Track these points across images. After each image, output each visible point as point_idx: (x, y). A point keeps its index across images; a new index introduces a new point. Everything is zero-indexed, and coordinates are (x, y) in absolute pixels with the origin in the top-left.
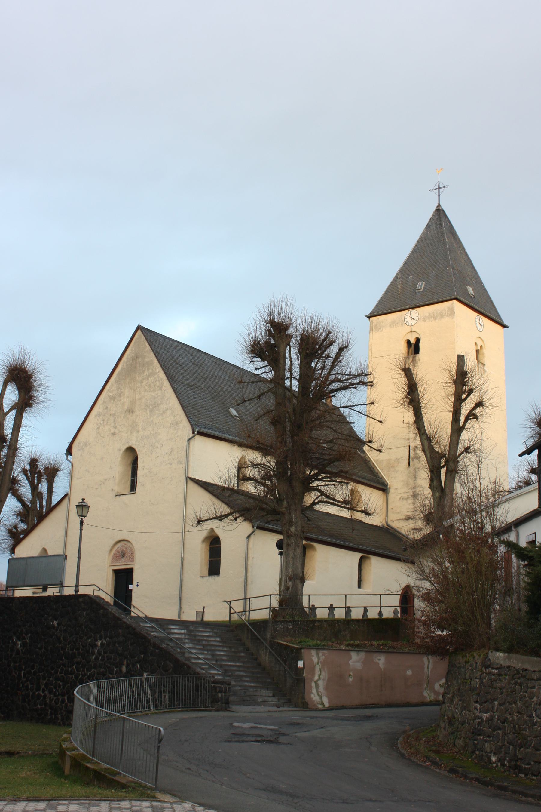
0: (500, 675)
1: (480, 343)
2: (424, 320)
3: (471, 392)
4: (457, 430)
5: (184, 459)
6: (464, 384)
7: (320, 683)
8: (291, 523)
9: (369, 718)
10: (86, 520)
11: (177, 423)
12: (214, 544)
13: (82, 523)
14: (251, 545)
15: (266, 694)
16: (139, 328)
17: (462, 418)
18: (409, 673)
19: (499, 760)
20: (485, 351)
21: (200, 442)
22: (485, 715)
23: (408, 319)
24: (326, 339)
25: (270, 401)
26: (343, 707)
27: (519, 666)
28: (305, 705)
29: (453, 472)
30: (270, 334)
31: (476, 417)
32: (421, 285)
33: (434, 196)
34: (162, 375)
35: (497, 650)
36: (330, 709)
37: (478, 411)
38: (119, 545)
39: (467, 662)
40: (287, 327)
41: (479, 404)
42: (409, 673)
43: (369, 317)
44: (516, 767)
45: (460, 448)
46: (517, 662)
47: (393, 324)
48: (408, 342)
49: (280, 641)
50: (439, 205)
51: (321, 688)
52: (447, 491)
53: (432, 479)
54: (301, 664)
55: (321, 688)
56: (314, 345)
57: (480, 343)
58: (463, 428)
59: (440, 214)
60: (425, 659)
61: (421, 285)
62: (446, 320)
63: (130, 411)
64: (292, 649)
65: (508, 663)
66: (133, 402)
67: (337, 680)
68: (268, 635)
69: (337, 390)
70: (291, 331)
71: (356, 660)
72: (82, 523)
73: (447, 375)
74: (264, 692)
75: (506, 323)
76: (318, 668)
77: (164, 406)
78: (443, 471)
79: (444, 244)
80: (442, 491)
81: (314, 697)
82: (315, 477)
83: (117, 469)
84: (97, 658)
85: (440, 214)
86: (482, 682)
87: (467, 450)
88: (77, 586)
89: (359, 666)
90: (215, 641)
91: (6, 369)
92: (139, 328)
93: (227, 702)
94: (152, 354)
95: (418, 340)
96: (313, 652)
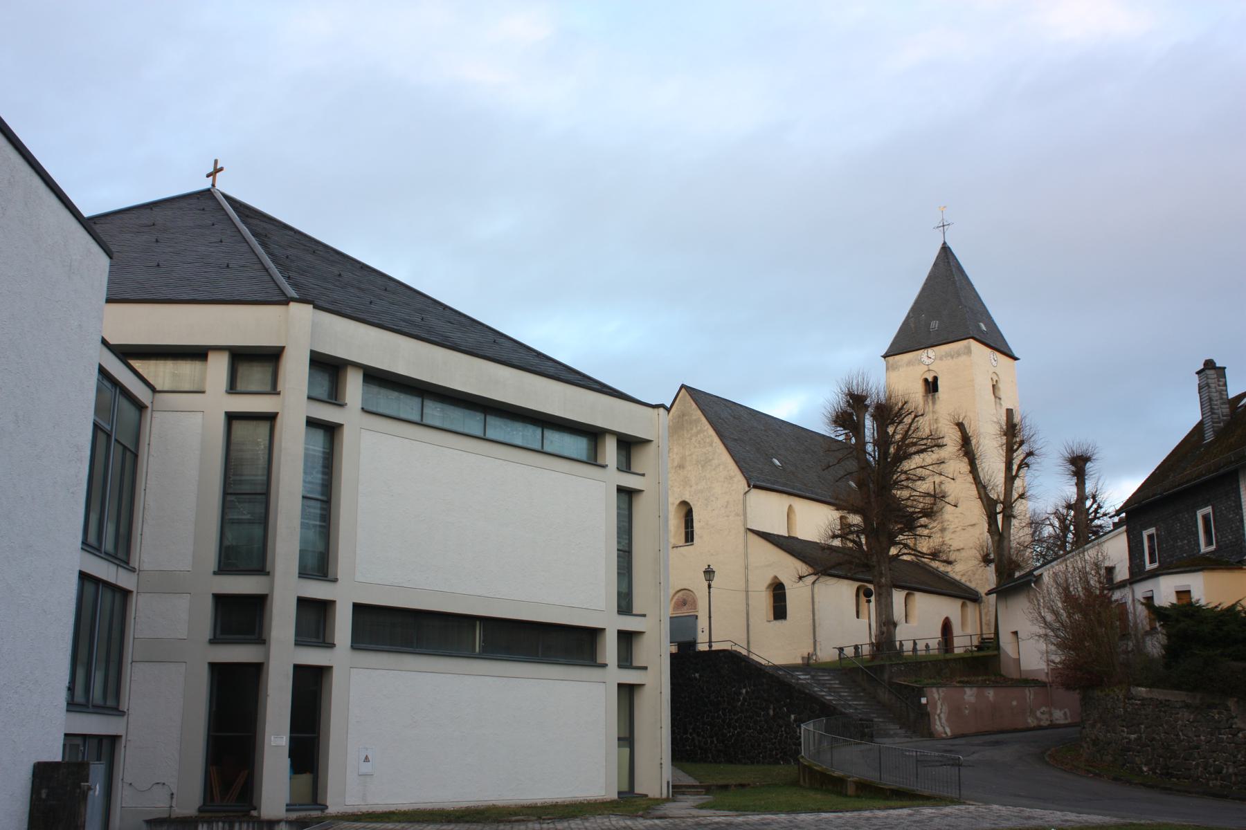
0: (1143, 705)
1: (995, 378)
2: (941, 359)
3: (1022, 443)
4: (1010, 479)
5: (741, 512)
6: (1014, 436)
7: (942, 715)
8: (881, 575)
9: (996, 743)
10: (713, 584)
11: (731, 478)
12: (778, 591)
13: (709, 586)
14: (816, 590)
15: (893, 728)
16: (683, 386)
17: (1015, 467)
18: (1014, 703)
19: (1150, 770)
20: (1000, 385)
21: (758, 496)
22: (1133, 737)
23: (925, 358)
24: (902, 408)
25: (852, 465)
26: (963, 736)
27: (1161, 697)
28: (931, 735)
29: (1008, 517)
30: (849, 405)
31: (1028, 465)
32: (935, 324)
33: (939, 232)
34: (711, 432)
35: (1139, 685)
36: (954, 737)
37: (1030, 460)
38: (680, 594)
39: (1107, 695)
40: (865, 398)
41: (1030, 454)
42: (1014, 703)
43: (885, 357)
44: (1168, 774)
45: (1015, 495)
46: (1159, 694)
47: (909, 363)
48: (926, 380)
49: (885, 681)
50: (945, 243)
51: (943, 720)
52: (1005, 535)
53: (990, 525)
54: (924, 701)
55: (943, 720)
56: (887, 413)
57: (995, 378)
58: (1017, 476)
59: (945, 250)
60: (1027, 691)
61: (935, 324)
62: (963, 358)
63: (681, 466)
64: (913, 689)
65: (1150, 696)
66: (683, 458)
67: (956, 712)
68: (886, 677)
69: (915, 453)
70: (868, 402)
71: (970, 694)
72: (709, 586)
73: (997, 427)
74: (892, 726)
75: (1016, 355)
76: (939, 703)
77: (715, 462)
78: (1000, 517)
79: (954, 283)
80: (1001, 535)
81: (938, 728)
82: (901, 532)
83: (675, 523)
84: (743, 704)
85: (945, 250)
86: (1126, 711)
87: (1022, 496)
88: (710, 642)
89: (973, 699)
90: (836, 684)
91: (1088, 589)
92: (683, 386)
93: (872, 736)
94: (699, 412)
95: (936, 379)
96: (934, 690)
